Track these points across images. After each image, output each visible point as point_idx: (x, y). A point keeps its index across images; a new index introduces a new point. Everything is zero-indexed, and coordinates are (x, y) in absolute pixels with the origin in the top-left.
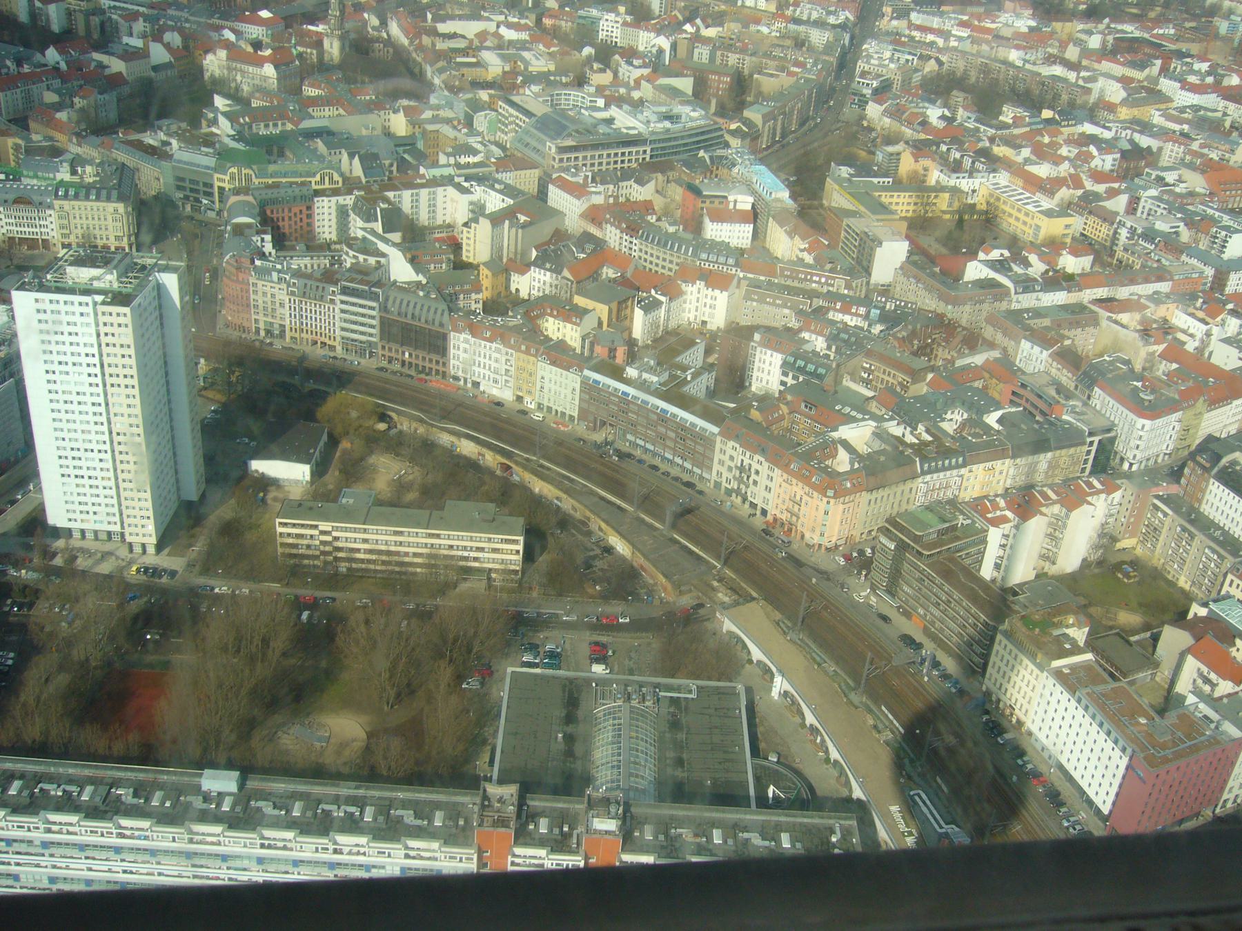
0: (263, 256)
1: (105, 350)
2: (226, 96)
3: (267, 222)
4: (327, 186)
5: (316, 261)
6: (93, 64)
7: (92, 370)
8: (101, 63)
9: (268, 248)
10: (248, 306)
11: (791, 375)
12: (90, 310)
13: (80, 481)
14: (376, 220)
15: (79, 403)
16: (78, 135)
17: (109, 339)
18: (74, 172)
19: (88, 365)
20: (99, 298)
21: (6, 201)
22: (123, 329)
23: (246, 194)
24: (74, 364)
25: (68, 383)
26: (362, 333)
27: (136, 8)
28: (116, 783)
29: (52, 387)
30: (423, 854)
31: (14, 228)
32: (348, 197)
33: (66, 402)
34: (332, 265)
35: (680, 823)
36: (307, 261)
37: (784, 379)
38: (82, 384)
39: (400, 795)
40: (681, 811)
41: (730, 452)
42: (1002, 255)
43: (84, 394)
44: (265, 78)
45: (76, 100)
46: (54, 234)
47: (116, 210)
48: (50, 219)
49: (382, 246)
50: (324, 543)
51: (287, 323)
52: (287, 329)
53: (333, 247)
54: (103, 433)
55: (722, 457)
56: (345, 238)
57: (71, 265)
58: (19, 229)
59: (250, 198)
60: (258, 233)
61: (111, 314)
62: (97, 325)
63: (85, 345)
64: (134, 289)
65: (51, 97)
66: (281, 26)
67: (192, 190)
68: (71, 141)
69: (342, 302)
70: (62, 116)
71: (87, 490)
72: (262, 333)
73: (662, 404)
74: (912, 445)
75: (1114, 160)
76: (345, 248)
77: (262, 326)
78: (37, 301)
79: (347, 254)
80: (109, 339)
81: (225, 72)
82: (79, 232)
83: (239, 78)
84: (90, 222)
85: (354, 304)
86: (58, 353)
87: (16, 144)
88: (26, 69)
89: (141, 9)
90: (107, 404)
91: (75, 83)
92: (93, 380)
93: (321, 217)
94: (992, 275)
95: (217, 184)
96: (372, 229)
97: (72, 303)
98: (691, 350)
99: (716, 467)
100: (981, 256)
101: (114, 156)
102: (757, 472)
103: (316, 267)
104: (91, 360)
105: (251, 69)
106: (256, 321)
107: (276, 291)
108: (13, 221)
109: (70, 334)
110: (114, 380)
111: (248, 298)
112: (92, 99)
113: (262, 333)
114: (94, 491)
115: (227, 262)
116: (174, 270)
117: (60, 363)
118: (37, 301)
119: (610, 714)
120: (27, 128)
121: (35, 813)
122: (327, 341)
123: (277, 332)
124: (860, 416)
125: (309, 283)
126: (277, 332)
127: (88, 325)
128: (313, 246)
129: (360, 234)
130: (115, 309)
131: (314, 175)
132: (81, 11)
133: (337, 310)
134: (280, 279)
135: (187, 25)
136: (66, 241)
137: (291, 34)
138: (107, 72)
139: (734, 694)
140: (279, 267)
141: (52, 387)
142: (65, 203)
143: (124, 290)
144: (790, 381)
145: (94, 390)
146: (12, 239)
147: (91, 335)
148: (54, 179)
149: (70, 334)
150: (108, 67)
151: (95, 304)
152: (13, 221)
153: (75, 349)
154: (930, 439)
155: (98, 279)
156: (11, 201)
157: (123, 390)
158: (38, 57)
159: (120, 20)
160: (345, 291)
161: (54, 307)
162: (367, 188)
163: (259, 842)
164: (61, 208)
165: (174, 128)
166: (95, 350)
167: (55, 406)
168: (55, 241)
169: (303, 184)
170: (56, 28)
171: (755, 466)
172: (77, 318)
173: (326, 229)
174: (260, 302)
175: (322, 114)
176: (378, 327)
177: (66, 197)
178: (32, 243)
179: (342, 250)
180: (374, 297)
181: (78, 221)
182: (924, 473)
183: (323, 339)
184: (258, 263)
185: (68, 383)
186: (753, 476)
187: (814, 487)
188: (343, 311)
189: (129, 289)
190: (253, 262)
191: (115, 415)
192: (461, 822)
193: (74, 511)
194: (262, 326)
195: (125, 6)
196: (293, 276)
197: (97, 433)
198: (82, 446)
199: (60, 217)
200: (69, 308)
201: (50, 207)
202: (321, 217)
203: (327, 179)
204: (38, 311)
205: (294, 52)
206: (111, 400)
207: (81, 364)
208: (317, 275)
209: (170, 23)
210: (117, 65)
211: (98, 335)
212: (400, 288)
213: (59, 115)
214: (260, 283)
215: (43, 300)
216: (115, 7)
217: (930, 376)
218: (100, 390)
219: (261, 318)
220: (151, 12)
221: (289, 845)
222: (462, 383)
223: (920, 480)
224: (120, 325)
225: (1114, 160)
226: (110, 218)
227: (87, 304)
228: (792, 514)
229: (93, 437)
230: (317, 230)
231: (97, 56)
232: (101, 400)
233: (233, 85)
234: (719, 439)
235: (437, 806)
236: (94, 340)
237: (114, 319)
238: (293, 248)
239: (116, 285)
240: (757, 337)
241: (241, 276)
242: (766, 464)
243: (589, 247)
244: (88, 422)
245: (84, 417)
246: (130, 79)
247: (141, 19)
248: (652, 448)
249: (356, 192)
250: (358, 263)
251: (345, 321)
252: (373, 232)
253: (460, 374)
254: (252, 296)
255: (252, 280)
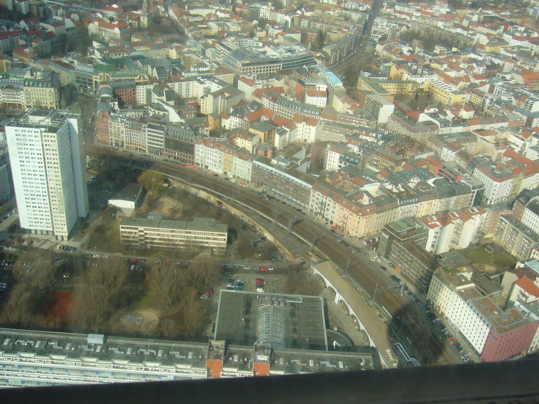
0: (114, 111)
1: (46, 152)
2: (98, 41)
3: (116, 96)
4: (142, 81)
5: (137, 113)
6: (41, 28)
7: (40, 161)
8: (44, 27)
9: (116, 107)
10: (108, 133)
11: (343, 163)
12: (39, 134)
13: (35, 209)
14: (163, 96)
15: (34, 175)
16: (34, 58)
17: (48, 147)
18: (32, 75)
19: (38, 158)
20: (43, 129)
21: (2, 87)
22: (53, 143)
23: (107, 84)
24: (32, 158)
25: (30, 166)
26: (157, 145)
27: (59, 3)
28: (50, 340)
29: (23, 168)
30: (184, 371)
31: (6, 99)
32: (151, 86)
33: (29, 174)
34: (144, 115)
35: (295, 357)
36: (133, 113)
37: (340, 164)
38: (36, 167)
39: (174, 345)
40: (295, 352)
41: (317, 196)
42: (435, 111)
43: (37, 171)
44: (115, 34)
45: (33, 43)
46: (23, 101)
47: (50, 91)
48: (21, 95)
49: (166, 107)
50: (141, 236)
51: (125, 140)
52: (125, 143)
53: (145, 107)
54: (45, 188)
55: (313, 198)
56: (150, 103)
57: (31, 115)
58: (8, 99)
59: (108, 86)
60: (112, 101)
61: (48, 136)
62: (42, 141)
63: (37, 150)
64: (58, 126)
65: (22, 42)
66: (122, 11)
67: (83, 83)
68: (31, 61)
69: (149, 131)
70: (27, 50)
71: (38, 213)
72: (114, 145)
73: (287, 175)
74: (396, 193)
75: (484, 69)
76: (150, 108)
77: (114, 141)
78: (16, 130)
79: (151, 110)
80: (48, 147)
81: (98, 31)
82: (34, 101)
83: (104, 34)
84: (39, 96)
85: (154, 132)
86: (25, 153)
87: (7, 63)
88: (11, 30)
89: (61, 4)
90: (46, 176)
91: (33, 36)
92: (40, 165)
93: (139, 94)
94: (431, 119)
95: (94, 80)
96: (162, 99)
97: (31, 132)
98: (300, 152)
99: (311, 203)
100: (426, 111)
101: (49, 67)
102: (329, 205)
103: (137, 116)
104: (39, 156)
105: (109, 30)
106: (111, 139)
107: (120, 126)
108: (5, 96)
109: (30, 145)
110: (50, 165)
111: (108, 129)
112: (40, 43)
113: (114, 145)
114: (41, 213)
115: (99, 114)
116: (76, 117)
117: (26, 158)
118: (16, 130)
119: (265, 310)
120: (12, 56)
121: (15, 353)
122: (142, 148)
123: (120, 144)
124: (373, 181)
125: (134, 123)
126: (120, 144)
127: (38, 141)
128: (136, 107)
129: (156, 101)
130: (50, 134)
131: (136, 76)
132: (35, 5)
133: (146, 135)
134: (121, 121)
135: (81, 11)
136: (29, 105)
137: (126, 15)
138: (47, 31)
139: (318, 301)
140: (121, 116)
141: (23, 168)
142: (28, 88)
143: (54, 126)
144: (343, 165)
145: (41, 169)
146: (5, 104)
147: (39, 145)
148: (24, 78)
149: (30, 145)
150: (47, 29)
151: (41, 132)
152: (5, 96)
153: (32, 151)
154: (404, 190)
155: (43, 121)
156: (5, 87)
157: (53, 169)
158: (17, 25)
159: (52, 9)
160: (150, 126)
161: (24, 133)
162: (159, 82)
163: (112, 365)
164: (27, 90)
165: (75, 55)
166: (41, 152)
167: (24, 176)
168: (24, 105)
169: (131, 80)
170: (24, 12)
171: (328, 202)
172: (33, 138)
173: (142, 100)
174: (113, 131)
175: (140, 49)
176: (164, 142)
177: (29, 85)
178: (14, 106)
179: (148, 109)
180: (162, 129)
181: (34, 96)
182: (401, 205)
183: (140, 147)
184: (112, 114)
185: (30, 166)
186: (327, 207)
187: (353, 211)
188: (149, 135)
189: (56, 125)
190: (110, 114)
191: (50, 180)
192: (200, 357)
193: (32, 222)
194: (114, 141)
195: (54, 2)
196: (127, 120)
197: (42, 188)
198: (36, 194)
199: (26, 94)
200: (30, 134)
201: (22, 90)
202: (139, 94)
203: (142, 78)
204: (17, 135)
205: (128, 22)
206: (48, 174)
207: (35, 158)
208: (138, 119)
209: (74, 10)
210: (51, 28)
211: (43, 145)
212: (174, 125)
213: (25, 50)
214: (113, 123)
215: (19, 130)
216: (50, 3)
217: (404, 163)
218: (43, 169)
219: (113, 138)
220: (65, 5)
221: (125, 367)
222: (200, 166)
223: (399, 208)
224: (52, 141)
225: (484, 69)
226: (48, 95)
227: (38, 132)
228: (344, 223)
229: (40, 189)
230: (138, 100)
231: (42, 24)
232: (44, 173)
233: (101, 37)
234: (312, 190)
235: (190, 350)
236: (41, 148)
237: (49, 139)
238: (127, 108)
239: (50, 124)
240: (328, 146)
241: (105, 120)
242: (332, 202)
243: (256, 107)
244: (38, 183)
245: (37, 181)
246: (56, 34)
247: (61, 8)
248: (283, 194)
249: (154, 83)
250: (155, 114)
251: (150, 139)
252: (162, 101)
253: (200, 162)
254: (110, 129)
255: (109, 122)
